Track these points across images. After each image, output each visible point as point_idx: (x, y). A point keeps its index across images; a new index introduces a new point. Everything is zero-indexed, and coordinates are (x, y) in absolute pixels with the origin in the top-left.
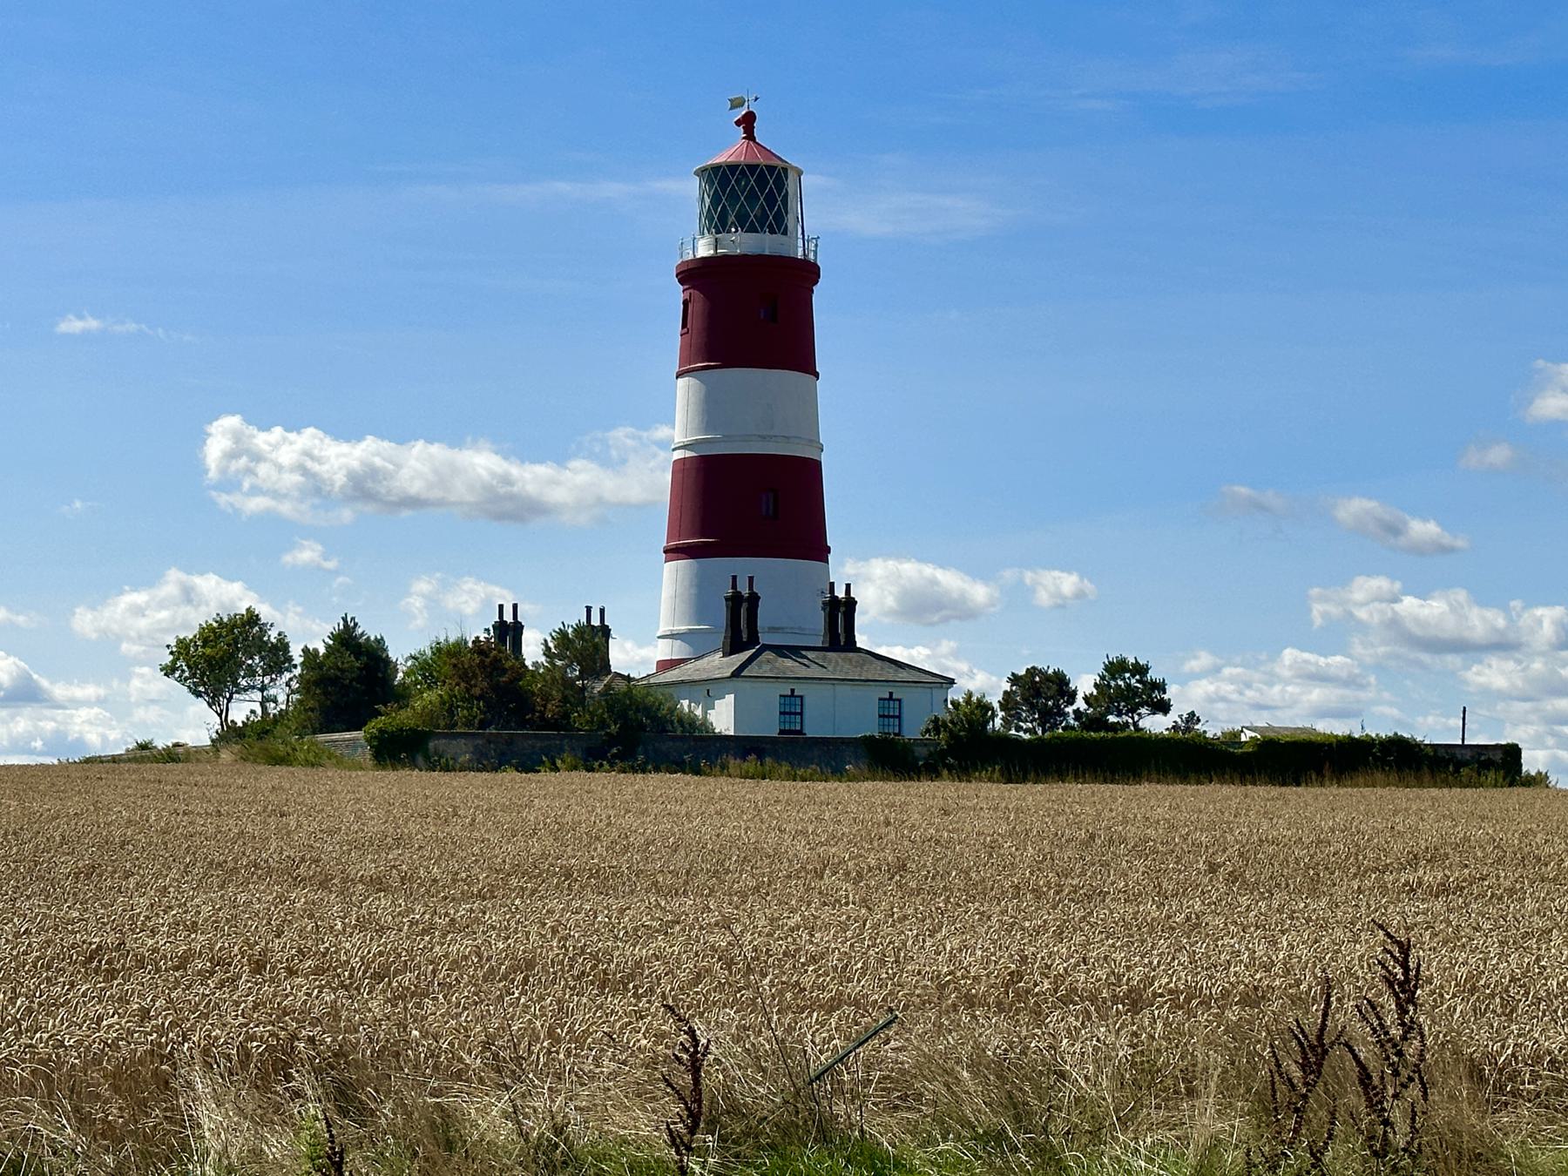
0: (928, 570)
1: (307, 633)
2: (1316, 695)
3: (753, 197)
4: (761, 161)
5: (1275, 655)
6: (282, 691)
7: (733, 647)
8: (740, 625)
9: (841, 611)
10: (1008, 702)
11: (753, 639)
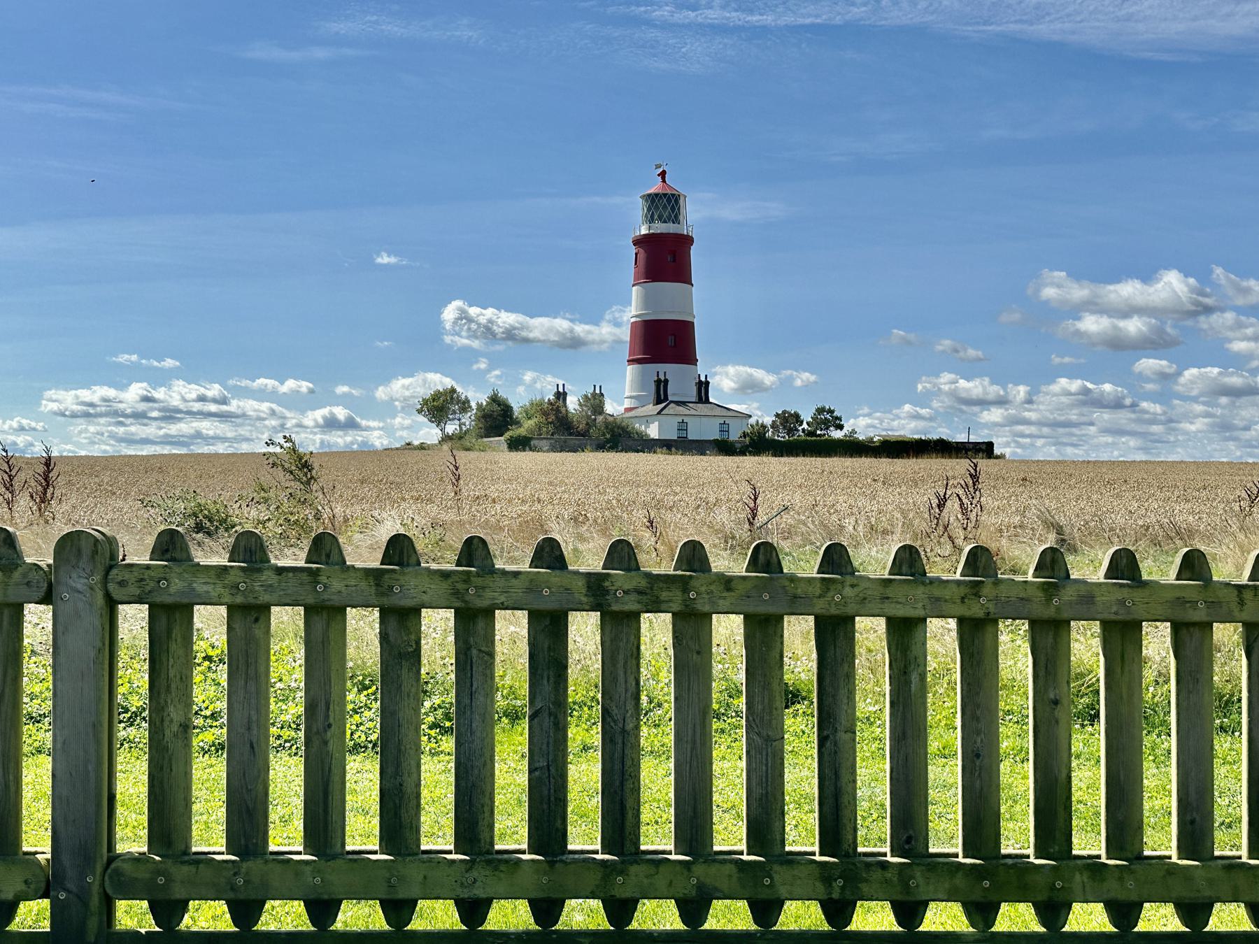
0: (749, 370)
1: (478, 397)
2: (913, 424)
3: (665, 207)
4: (669, 192)
5: (900, 405)
6: (468, 420)
7: (658, 402)
8: (661, 393)
9: (703, 387)
10: (774, 425)
11: (666, 398)
